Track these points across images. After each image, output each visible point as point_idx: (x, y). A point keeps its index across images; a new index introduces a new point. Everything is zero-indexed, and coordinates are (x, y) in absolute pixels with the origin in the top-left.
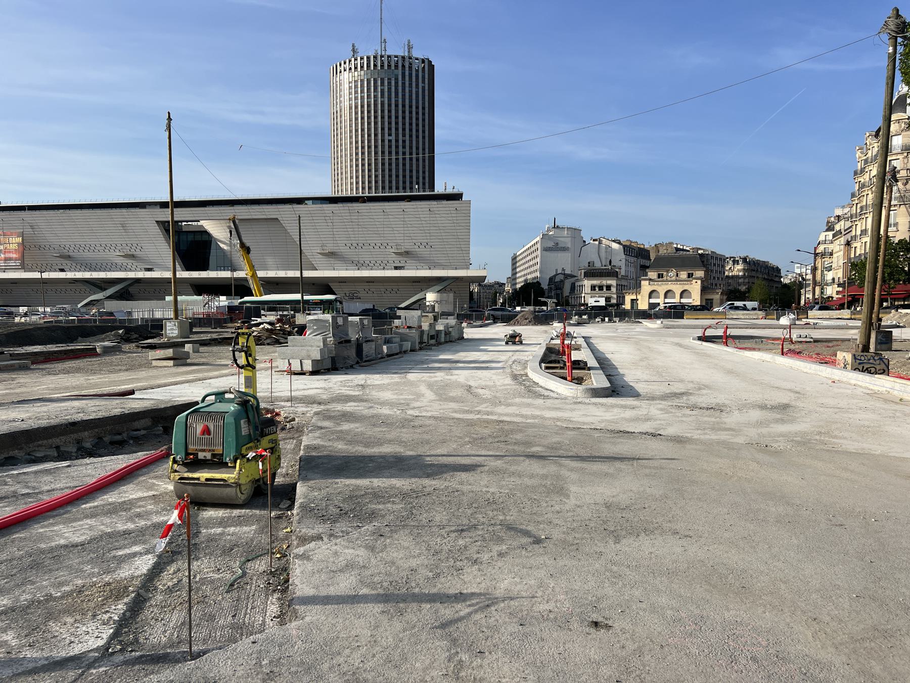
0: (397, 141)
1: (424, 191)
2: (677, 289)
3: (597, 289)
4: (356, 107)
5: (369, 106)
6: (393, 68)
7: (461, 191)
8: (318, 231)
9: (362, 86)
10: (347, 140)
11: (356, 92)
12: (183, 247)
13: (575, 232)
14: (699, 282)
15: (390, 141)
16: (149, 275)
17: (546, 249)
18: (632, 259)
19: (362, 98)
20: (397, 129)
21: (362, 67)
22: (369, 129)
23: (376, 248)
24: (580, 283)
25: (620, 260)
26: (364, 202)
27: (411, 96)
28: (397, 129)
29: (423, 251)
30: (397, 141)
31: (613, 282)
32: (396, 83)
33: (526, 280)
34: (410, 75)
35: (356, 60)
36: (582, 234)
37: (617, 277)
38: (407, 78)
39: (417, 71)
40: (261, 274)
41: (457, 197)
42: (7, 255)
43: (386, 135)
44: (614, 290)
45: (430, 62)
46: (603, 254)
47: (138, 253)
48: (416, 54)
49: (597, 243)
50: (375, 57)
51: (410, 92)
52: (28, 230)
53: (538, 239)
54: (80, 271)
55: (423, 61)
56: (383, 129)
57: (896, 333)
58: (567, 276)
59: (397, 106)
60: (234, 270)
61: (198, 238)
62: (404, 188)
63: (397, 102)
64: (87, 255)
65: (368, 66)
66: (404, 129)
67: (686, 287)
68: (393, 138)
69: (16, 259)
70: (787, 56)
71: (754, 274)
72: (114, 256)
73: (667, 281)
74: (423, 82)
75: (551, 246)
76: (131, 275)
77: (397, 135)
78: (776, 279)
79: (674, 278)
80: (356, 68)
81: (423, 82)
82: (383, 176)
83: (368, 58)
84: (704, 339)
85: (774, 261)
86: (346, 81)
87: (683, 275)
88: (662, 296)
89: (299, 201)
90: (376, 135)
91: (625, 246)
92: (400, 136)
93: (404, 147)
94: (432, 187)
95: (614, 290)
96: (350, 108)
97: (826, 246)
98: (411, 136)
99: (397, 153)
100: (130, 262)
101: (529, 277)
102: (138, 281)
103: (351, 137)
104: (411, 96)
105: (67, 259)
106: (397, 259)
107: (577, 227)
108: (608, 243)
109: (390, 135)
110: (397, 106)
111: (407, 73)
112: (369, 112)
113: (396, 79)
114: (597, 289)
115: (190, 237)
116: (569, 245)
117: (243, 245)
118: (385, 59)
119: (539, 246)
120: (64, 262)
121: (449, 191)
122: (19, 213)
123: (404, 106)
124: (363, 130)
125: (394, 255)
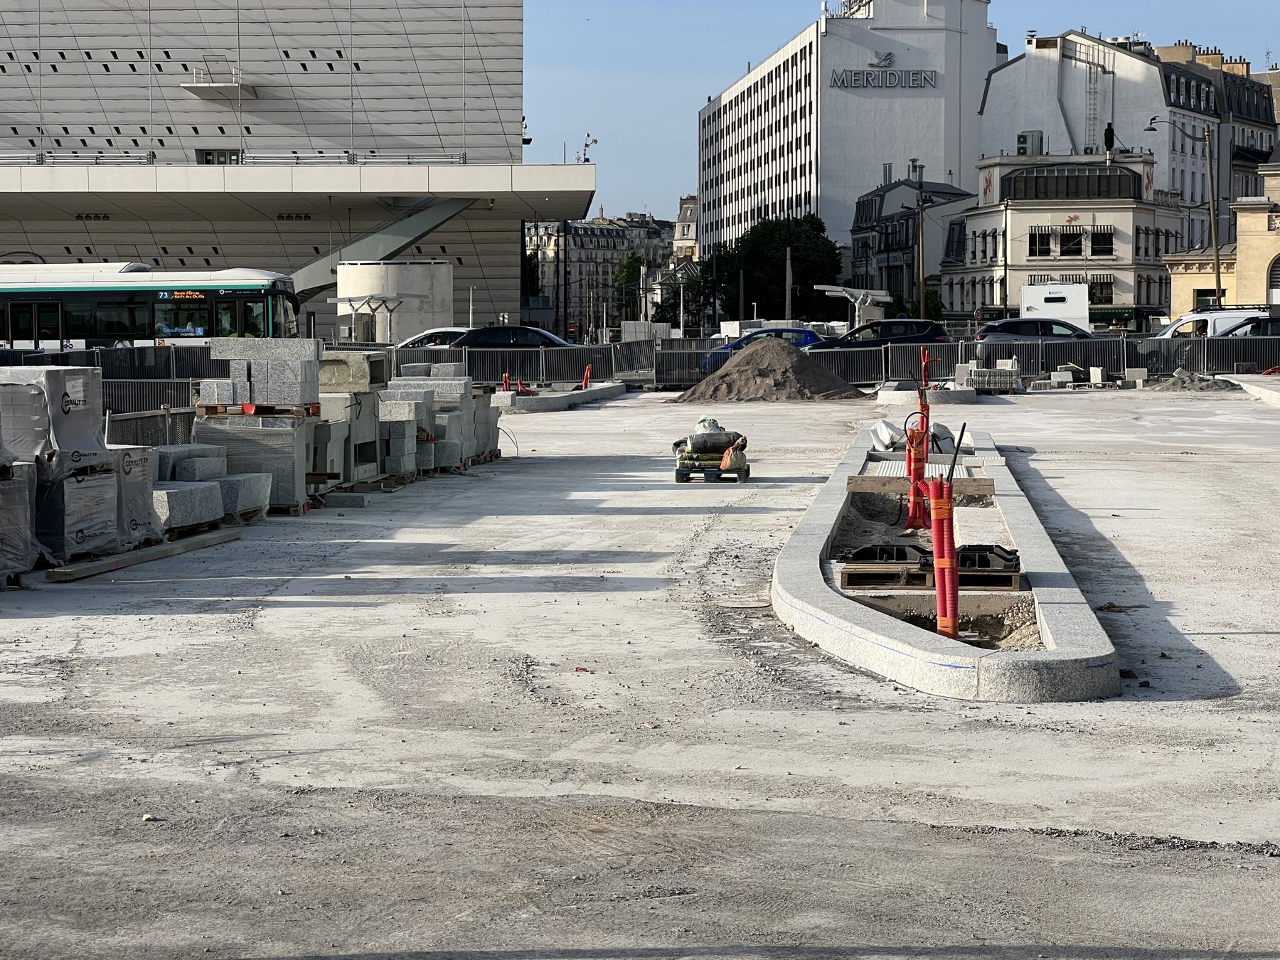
3: (1055, 247)
12: (1231, 247)
24: (987, 224)
25: (1150, 130)
29: (319, 85)
31: (1119, 219)
33: (760, 211)
37: (1138, 197)
44: (1123, 250)
46: (1079, 103)
49: (1053, 54)
53: (809, 36)
58: (931, 194)
75: (869, 71)
91: (1169, 72)
114: (1055, 247)
119: (813, 63)
125: (195, 102)
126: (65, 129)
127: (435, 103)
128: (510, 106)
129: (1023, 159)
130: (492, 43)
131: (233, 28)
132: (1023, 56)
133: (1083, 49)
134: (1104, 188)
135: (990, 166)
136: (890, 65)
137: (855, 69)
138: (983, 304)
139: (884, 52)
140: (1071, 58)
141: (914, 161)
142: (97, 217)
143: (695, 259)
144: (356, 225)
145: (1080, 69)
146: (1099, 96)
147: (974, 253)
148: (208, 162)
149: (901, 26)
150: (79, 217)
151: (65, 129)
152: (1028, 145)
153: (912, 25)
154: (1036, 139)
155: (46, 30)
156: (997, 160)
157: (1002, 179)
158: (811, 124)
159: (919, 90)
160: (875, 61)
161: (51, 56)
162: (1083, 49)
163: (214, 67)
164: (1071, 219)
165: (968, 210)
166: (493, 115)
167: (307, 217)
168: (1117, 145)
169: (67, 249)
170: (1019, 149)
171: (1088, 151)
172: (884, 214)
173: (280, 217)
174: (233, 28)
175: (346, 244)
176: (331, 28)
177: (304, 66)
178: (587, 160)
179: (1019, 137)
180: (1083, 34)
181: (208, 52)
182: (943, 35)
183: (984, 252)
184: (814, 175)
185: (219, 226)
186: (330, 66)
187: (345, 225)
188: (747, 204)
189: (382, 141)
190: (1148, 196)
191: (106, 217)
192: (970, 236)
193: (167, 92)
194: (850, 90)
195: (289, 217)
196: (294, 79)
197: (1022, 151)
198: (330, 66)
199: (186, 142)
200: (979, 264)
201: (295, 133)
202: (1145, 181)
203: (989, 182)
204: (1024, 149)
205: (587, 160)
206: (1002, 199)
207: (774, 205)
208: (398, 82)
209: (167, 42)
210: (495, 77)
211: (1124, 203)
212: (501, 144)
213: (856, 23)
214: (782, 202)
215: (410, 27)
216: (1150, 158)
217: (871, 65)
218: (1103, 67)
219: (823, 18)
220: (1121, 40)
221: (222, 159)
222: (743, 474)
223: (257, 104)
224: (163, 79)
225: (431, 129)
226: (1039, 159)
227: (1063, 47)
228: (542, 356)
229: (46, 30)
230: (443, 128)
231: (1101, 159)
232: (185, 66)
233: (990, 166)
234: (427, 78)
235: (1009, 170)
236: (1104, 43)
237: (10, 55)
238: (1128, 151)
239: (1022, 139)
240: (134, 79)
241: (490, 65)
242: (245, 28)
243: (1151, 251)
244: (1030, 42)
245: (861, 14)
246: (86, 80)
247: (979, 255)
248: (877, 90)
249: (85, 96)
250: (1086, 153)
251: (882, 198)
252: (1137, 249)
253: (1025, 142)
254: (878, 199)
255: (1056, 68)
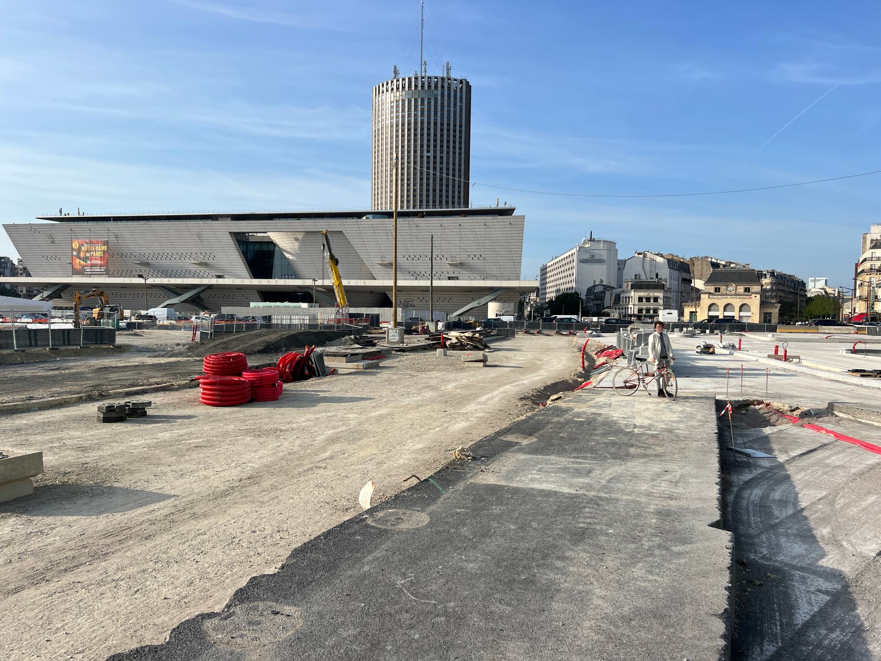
0: (435, 157)
1: (434, 206)
2: (737, 302)
3: (644, 300)
4: (397, 125)
5: (409, 124)
6: (433, 88)
7: (513, 206)
8: (371, 245)
9: (403, 105)
10: (387, 159)
11: (397, 111)
12: (250, 257)
13: (611, 245)
14: (758, 296)
15: (428, 157)
16: (221, 281)
17: (582, 261)
18: (677, 273)
19: (403, 117)
20: (435, 146)
21: (403, 88)
22: (409, 146)
23: (430, 257)
24: (627, 295)
25: (665, 273)
26: (423, 217)
27: (449, 115)
28: (435, 146)
29: (476, 263)
30: (435, 157)
31: (660, 294)
32: (436, 103)
33: (558, 291)
34: (449, 95)
35: (398, 81)
36: (617, 247)
38: (446, 98)
39: (455, 91)
40: (345, 283)
41: (508, 212)
42: (94, 262)
43: (425, 152)
45: (468, 83)
46: (647, 267)
47: (211, 261)
48: (454, 75)
49: (641, 256)
50: (416, 78)
51: (449, 111)
52: (112, 239)
54: (157, 277)
55: (461, 82)
56: (422, 146)
58: (607, 288)
59: (435, 124)
60: (296, 276)
61: (265, 248)
62: (459, 204)
63: (436, 120)
64: (164, 262)
65: (410, 87)
66: (442, 146)
67: (745, 301)
68: (431, 154)
69: (101, 266)
70: (796, 72)
71: (781, 287)
72: (189, 264)
73: (726, 295)
74: (461, 101)
75: (588, 259)
76: (206, 281)
77: (435, 151)
78: (802, 293)
79: (733, 292)
80: (398, 89)
81: (461, 101)
82: (421, 191)
83: (410, 79)
84: (854, 351)
85: (799, 276)
86: (388, 100)
87: (741, 289)
88: (721, 309)
89: (359, 215)
90: (415, 152)
91: (668, 260)
92: (438, 152)
93: (441, 163)
94: (466, 203)
95: (661, 301)
96: (392, 126)
97: (873, 263)
98: (448, 153)
99: (435, 169)
100: (202, 269)
101: (562, 287)
102: (210, 287)
103: (391, 154)
104: (449, 115)
105: (146, 265)
107: (612, 240)
108: (652, 256)
109: (428, 151)
110: (435, 124)
111: (446, 93)
112: (409, 130)
113: (436, 99)
114: (644, 300)
115: (257, 247)
117: (332, 257)
118: (426, 80)
119: (575, 257)
120: (143, 268)
121: (501, 206)
122: (105, 223)
123: (442, 124)
124: (403, 147)
188: (554, 289)
222: (713, 353)
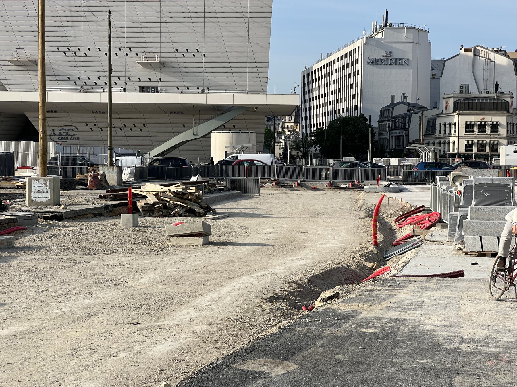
3: (476, 130)
13: (420, 35)
24: (447, 120)
29: (189, 62)
31: (502, 119)
33: (332, 113)
37: (507, 110)
44: (503, 131)
46: (481, 73)
49: (471, 54)
53: (358, 44)
57: (47, 118)
95: (503, 131)
106: (145, 74)
107: (422, 27)
114: (476, 130)
116: (410, 56)
125: (140, 68)
126: (89, 78)
127: (234, 70)
128: (263, 71)
129: (462, 95)
130: (257, 47)
131: (158, 40)
132: (458, 55)
133: (483, 52)
134: (483, 107)
135: (449, 98)
136: (390, 56)
137: (377, 57)
138: (444, 151)
139: (388, 51)
140: (478, 56)
141: (403, 94)
142: (100, 112)
143: (298, 130)
144: (202, 116)
145: (481, 60)
146: (489, 71)
147: (440, 131)
148: (143, 91)
149: (395, 41)
150: (93, 112)
151: (89, 78)
152: (464, 90)
153: (399, 41)
154: (467, 87)
155: (85, 39)
156: (452, 95)
157: (454, 103)
158: (359, 78)
159: (402, 66)
160: (385, 55)
161: (188, 55)
162: (483, 52)
163: (148, 55)
164: (482, 119)
165: (437, 114)
166: (256, 75)
167: (182, 113)
168: (499, 90)
169: (87, 124)
170: (460, 91)
171: (487, 92)
172: (393, 115)
173: (171, 113)
174: (158, 40)
175: (199, 124)
176: (195, 40)
177: (183, 55)
178: (295, 93)
179: (460, 87)
180: (482, 47)
181: (147, 49)
182: (411, 45)
183: (445, 131)
184: (359, 99)
185: (146, 116)
186: (194, 55)
187: (197, 116)
189: (212, 84)
190: (511, 110)
191: (55, 112)
192: (439, 124)
193: (129, 64)
194: (375, 65)
195: (175, 113)
196: (180, 60)
197: (461, 92)
198: (194, 55)
199: (135, 83)
200: (442, 136)
201: (179, 80)
202: (510, 105)
203: (448, 104)
204: (462, 91)
205: (295, 93)
206: (455, 110)
207: (339, 110)
208: (220, 61)
209: (130, 45)
210: (258, 60)
211: (503, 113)
212: (259, 86)
213: (378, 39)
214: (343, 109)
215: (226, 40)
216: (511, 95)
217: (383, 56)
218: (490, 60)
219: (365, 37)
220: (495, 49)
221: (149, 90)
223: (167, 69)
224: (128, 59)
225: (232, 79)
226: (468, 95)
227: (475, 52)
228: (360, 171)
229: (85, 39)
230: (236, 79)
231: (493, 95)
232: (137, 54)
233: (449, 98)
234: (231, 60)
235: (457, 99)
236: (489, 50)
237: (68, 48)
238: (503, 93)
239: (461, 87)
240: (66, 58)
241: (256, 55)
242: (163, 40)
243: (512, 132)
244: (461, 49)
245: (379, 36)
246: (98, 59)
247: (443, 132)
248: (385, 66)
249: (97, 65)
250: (486, 93)
251: (393, 109)
252: (508, 131)
253: (462, 88)
254: (391, 109)
255: (471, 60)
